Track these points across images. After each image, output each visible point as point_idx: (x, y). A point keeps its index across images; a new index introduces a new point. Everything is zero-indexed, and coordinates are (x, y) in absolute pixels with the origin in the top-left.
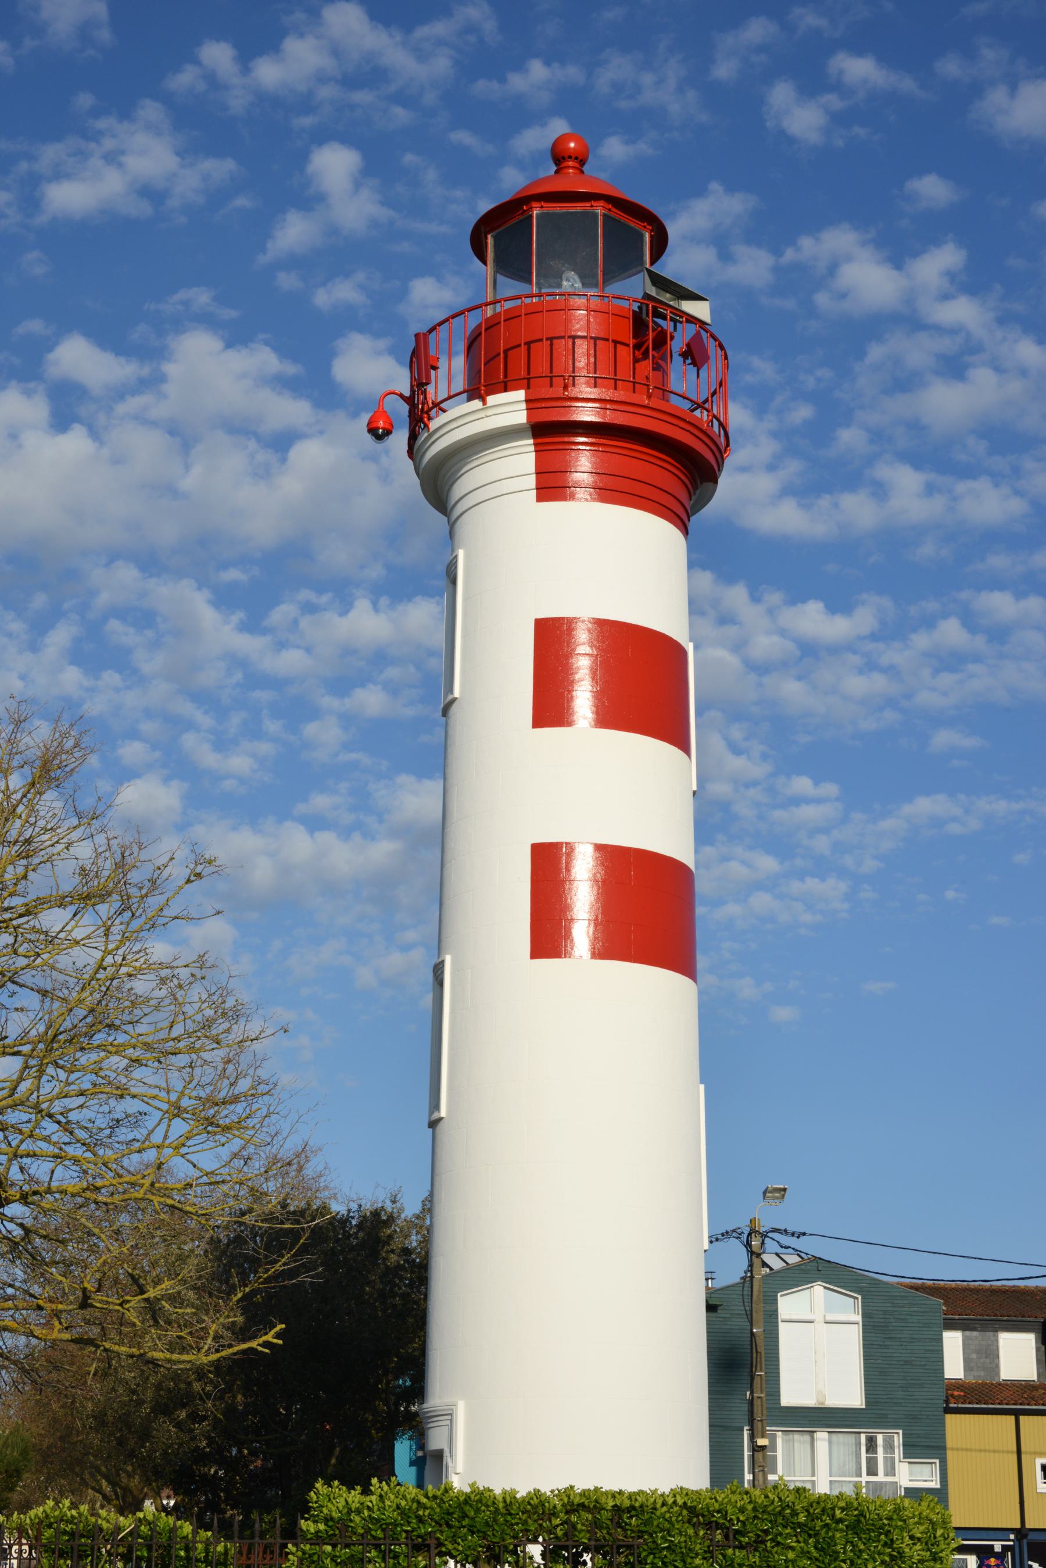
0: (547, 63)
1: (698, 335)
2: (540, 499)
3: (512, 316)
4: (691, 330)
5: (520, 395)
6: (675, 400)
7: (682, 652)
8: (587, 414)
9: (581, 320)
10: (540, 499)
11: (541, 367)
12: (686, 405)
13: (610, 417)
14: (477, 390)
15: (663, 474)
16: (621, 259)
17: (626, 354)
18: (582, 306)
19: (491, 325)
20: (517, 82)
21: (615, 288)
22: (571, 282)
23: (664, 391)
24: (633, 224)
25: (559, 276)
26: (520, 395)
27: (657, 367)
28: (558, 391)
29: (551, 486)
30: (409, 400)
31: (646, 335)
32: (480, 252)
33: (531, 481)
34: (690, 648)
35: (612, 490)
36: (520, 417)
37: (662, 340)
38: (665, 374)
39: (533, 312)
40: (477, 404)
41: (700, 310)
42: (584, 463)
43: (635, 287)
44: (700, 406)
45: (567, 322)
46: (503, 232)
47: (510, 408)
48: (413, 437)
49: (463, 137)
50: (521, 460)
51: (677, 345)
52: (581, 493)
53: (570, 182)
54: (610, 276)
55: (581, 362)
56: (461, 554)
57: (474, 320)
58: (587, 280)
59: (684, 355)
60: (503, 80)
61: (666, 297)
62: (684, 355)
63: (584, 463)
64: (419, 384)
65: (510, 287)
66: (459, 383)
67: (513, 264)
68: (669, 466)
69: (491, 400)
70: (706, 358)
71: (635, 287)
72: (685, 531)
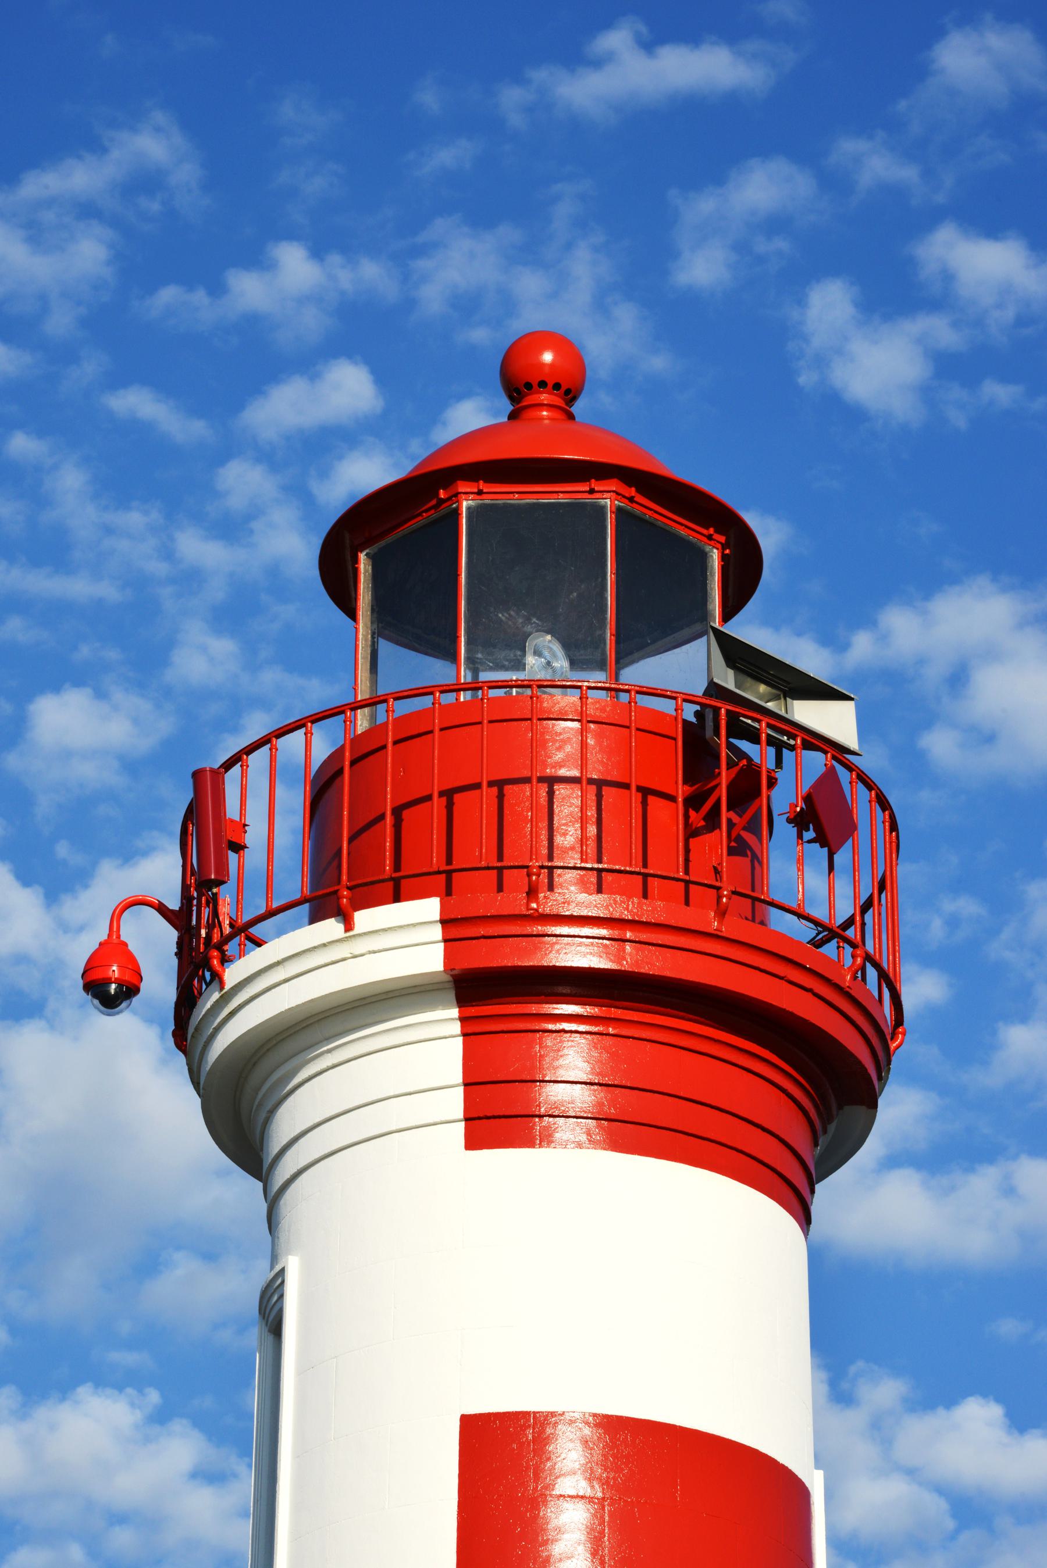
0: (317, 253)
1: (829, 777)
2: (473, 1142)
3: (411, 734)
4: (816, 762)
5: (430, 908)
6: (782, 923)
7: (799, 1493)
8: (579, 952)
9: (565, 744)
10: (473, 1142)
11: (476, 846)
12: (804, 932)
13: (631, 959)
14: (334, 893)
15: (754, 1088)
16: (658, 613)
17: (669, 818)
18: (566, 702)
19: (363, 753)
20: (249, 290)
21: (644, 671)
22: (544, 657)
23: (756, 902)
24: (684, 530)
25: (516, 647)
26: (430, 908)
27: (738, 848)
28: (515, 901)
29: (500, 1112)
30: (177, 918)
31: (715, 775)
32: (344, 598)
33: (454, 1103)
34: (815, 1483)
35: (634, 1125)
36: (428, 957)
37: (750, 785)
38: (758, 862)
39: (458, 723)
40: (331, 928)
41: (833, 720)
42: (572, 1063)
43: (682, 671)
44: (828, 933)
45: (537, 746)
46: (392, 551)
47: (405, 937)
48: (186, 1001)
49: (137, 403)
50: (433, 1048)
51: (783, 798)
52: (566, 1130)
53: (543, 437)
54: (634, 644)
55: (568, 837)
56: (293, 1266)
57: (323, 744)
58: (581, 651)
59: (800, 821)
60: (217, 289)
61: (757, 692)
62: (800, 821)
63: (572, 1063)
64: (201, 883)
65: (408, 667)
66: (292, 883)
67: (415, 615)
68: (772, 1071)
69: (365, 918)
70: (849, 829)
71: (682, 671)
72: (802, 1213)
